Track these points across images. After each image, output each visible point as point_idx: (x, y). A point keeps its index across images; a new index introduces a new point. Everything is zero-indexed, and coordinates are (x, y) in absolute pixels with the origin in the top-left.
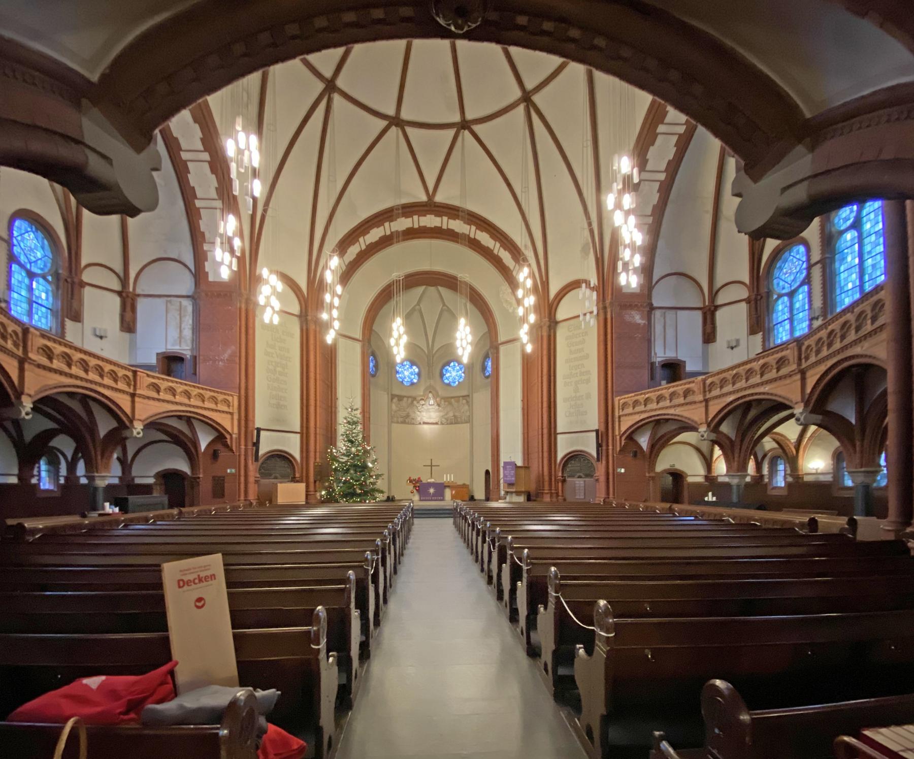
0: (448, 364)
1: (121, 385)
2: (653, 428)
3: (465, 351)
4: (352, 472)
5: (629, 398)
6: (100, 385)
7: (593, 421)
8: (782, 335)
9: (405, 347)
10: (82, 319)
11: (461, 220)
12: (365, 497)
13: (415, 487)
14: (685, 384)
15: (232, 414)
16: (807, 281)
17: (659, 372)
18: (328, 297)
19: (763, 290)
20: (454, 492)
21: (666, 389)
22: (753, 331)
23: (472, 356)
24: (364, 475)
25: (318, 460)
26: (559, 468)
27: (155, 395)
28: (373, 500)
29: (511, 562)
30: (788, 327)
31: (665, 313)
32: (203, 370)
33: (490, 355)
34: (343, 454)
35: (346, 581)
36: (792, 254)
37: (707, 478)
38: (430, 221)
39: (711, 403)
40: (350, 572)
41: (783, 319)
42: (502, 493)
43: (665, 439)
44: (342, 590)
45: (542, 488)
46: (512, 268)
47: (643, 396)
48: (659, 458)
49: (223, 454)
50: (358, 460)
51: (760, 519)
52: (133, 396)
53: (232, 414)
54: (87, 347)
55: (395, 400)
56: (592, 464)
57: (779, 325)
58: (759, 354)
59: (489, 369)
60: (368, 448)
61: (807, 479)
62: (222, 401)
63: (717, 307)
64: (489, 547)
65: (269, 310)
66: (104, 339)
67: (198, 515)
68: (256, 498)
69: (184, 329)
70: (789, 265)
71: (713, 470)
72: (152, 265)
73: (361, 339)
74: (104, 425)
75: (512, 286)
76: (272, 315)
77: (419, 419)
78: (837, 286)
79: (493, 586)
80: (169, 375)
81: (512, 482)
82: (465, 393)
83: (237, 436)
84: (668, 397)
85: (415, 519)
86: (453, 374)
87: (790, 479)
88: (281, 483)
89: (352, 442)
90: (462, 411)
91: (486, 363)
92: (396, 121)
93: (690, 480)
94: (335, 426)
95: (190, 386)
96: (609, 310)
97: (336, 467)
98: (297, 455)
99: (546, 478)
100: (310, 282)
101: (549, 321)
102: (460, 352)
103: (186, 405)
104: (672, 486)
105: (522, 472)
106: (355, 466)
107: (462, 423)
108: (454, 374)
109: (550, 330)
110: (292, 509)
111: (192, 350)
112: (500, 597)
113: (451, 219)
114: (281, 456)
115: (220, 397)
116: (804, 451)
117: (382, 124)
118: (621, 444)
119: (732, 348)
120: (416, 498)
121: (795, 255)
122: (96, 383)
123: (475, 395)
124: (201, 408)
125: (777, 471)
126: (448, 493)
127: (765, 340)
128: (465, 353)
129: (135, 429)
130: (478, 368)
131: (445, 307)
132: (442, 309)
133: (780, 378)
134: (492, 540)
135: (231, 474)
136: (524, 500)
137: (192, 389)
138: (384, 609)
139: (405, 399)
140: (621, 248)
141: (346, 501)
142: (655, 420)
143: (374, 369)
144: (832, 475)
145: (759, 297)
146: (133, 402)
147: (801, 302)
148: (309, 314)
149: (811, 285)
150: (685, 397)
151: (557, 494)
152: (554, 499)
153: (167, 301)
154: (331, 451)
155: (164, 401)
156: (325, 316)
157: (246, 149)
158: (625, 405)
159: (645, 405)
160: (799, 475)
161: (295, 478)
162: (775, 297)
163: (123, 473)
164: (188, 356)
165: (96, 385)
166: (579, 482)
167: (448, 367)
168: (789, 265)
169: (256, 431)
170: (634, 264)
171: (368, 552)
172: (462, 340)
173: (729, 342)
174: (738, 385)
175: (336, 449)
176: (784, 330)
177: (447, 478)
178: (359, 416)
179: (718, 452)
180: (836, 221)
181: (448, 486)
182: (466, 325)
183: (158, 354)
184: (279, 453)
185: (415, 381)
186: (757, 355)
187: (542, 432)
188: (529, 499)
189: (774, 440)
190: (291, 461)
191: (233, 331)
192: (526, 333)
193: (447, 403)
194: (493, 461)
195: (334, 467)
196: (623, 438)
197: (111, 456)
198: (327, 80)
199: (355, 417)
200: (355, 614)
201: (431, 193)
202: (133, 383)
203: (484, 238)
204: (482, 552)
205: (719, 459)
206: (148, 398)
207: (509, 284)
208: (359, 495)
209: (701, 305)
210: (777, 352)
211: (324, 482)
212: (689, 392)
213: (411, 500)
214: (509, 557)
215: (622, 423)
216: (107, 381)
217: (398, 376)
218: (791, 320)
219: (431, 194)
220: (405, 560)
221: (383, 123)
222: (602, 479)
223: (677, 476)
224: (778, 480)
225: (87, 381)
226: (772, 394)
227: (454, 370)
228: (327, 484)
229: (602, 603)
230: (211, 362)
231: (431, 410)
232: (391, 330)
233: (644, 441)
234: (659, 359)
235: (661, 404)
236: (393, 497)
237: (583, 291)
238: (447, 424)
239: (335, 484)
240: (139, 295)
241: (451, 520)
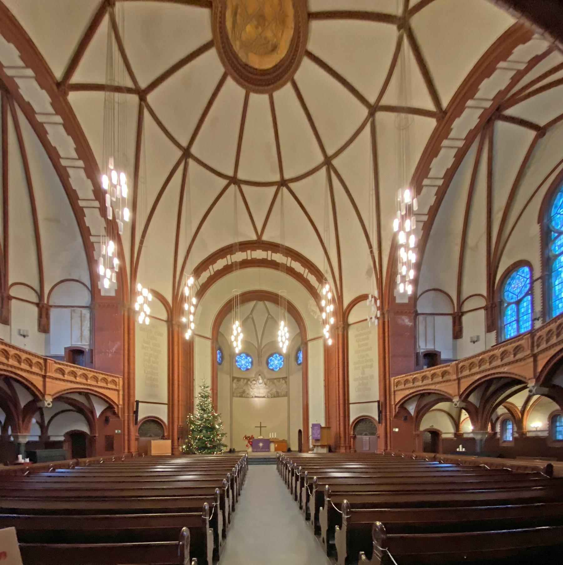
0: (272, 355)
1: (35, 369)
2: (419, 399)
5: (401, 378)
6: (19, 369)
7: (375, 394)
8: (511, 332)
10: (10, 324)
11: (281, 253)
12: (213, 450)
13: (249, 442)
14: (443, 367)
15: (118, 391)
16: (531, 292)
17: (422, 360)
18: (186, 306)
19: (497, 300)
20: (276, 446)
21: (428, 371)
22: (489, 329)
23: (290, 348)
24: (213, 434)
25: (180, 424)
26: (351, 428)
27: (61, 376)
28: (220, 452)
29: (328, 507)
30: (515, 326)
31: (426, 318)
33: (302, 349)
34: (198, 419)
35: (201, 509)
36: (519, 273)
37: (456, 435)
38: (259, 254)
39: (462, 381)
40: (205, 504)
41: (512, 321)
42: (311, 446)
43: (427, 407)
44: (177, 546)
45: (339, 443)
46: (316, 287)
47: (411, 376)
48: (422, 421)
49: (112, 419)
50: (209, 423)
51: (511, 466)
52: (44, 377)
53: (118, 391)
54: (13, 343)
55: (235, 381)
56: (375, 425)
57: (508, 325)
58: (494, 346)
60: (216, 415)
61: (529, 435)
62: (110, 381)
63: (463, 314)
66: (26, 338)
67: (90, 464)
68: (137, 451)
69: (84, 330)
70: (516, 282)
72: (60, 285)
73: (211, 338)
74: (24, 400)
75: (317, 300)
76: (145, 318)
77: (252, 394)
78: (553, 295)
79: (297, 501)
80: (74, 363)
82: (284, 376)
83: (122, 406)
84: (430, 376)
86: (276, 362)
87: (516, 435)
88: (154, 440)
90: (282, 388)
91: (298, 355)
92: (234, 180)
93: (444, 436)
95: (87, 370)
96: (386, 316)
97: (193, 429)
98: (165, 420)
99: (342, 435)
101: (343, 324)
102: (281, 345)
103: (84, 384)
104: (431, 441)
105: (325, 431)
106: (206, 428)
109: (344, 330)
110: (161, 459)
111: (90, 345)
112: (308, 518)
113: (274, 252)
114: (154, 421)
115: (110, 379)
116: (527, 415)
117: (225, 182)
118: (395, 411)
119: (474, 342)
120: (250, 450)
121: (521, 274)
122: (15, 367)
123: (291, 377)
124: (96, 386)
125: (506, 429)
126: (272, 446)
127: (498, 336)
130: (293, 358)
131: (270, 316)
133: (517, 361)
135: (118, 434)
136: (327, 451)
137: (89, 372)
138: (223, 544)
139: (242, 380)
140: (399, 265)
141: (200, 453)
143: (220, 359)
144: (548, 432)
145: (494, 305)
146: (44, 382)
147: (525, 308)
149: (534, 295)
150: (443, 377)
152: (348, 451)
153: (71, 310)
154: (190, 416)
155: (67, 381)
156: (184, 320)
158: (397, 384)
159: (413, 383)
160: (523, 432)
161: (164, 436)
162: (506, 305)
163: (42, 432)
164: (87, 350)
165: (15, 369)
166: (366, 438)
167: (272, 358)
168: (516, 282)
171: (217, 489)
172: (282, 336)
173: (471, 338)
174: (483, 367)
175: (193, 415)
176: (512, 329)
177: (272, 436)
178: (210, 392)
179: (464, 415)
180: (553, 248)
181: (273, 442)
182: (285, 326)
183: (65, 348)
184: (153, 419)
185: (249, 367)
186: (492, 347)
187: (339, 402)
188: (330, 451)
189: (505, 407)
191: (119, 331)
192: (327, 331)
194: (304, 424)
195: (191, 428)
196: (397, 406)
197: (30, 421)
198: (184, 149)
199: (207, 392)
200: (210, 532)
201: (259, 234)
202: (44, 368)
203: (297, 266)
204: (292, 481)
205: (466, 420)
206: (56, 379)
208: (209, 448)
209: (451, 312)
210: (515, 342)
211: (185, 439)
212: (446, 372)
213: (246, 451)
214: (326, 503)
215: (396, 396)
216: (24, 366)
217: (237, 364)
218: (518, 321)
223: (435, 434)
224: (507, 436)
225: (8, 365)
226: (510, 373)
227: (276, 359)
228: (187, 440)
229: (378, 523)
230: (103, 354)
232: (232, 330)
233: (412, 409)
234: (422, 351)
235: (425, 382)
236: (234, 449)
237: (369, 302)
238: (272, 397)
239: (192, 441)
240: (51, 306)
241: (275, 466)
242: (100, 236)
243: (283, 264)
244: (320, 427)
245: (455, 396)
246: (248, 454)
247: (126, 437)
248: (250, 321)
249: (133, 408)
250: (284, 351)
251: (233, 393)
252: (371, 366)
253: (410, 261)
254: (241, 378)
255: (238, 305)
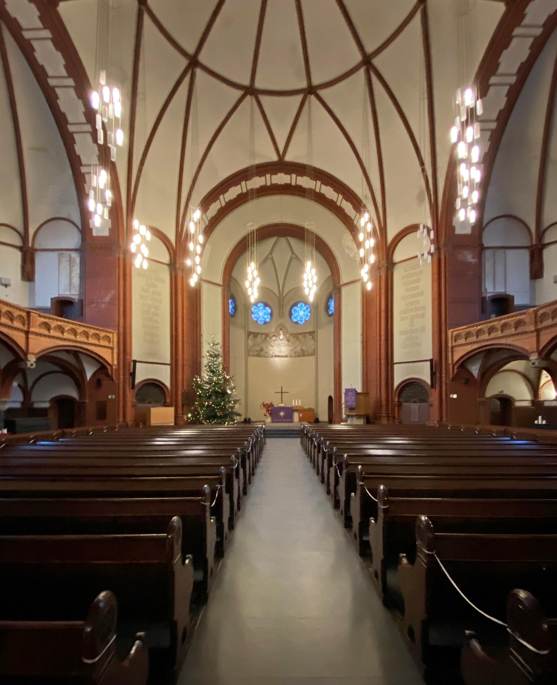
0: (296, 305)
1: (17, 324)
3: (311, 291)
4: (214, 397)
5: (462, 330)
9: (258, 288)
13: (268, 410)
15: (112, 348)
17: (489, 307)
18: (191, 246)
20: (301, 415)
21: (497, 322)
23: (318, 296)
24: (224, 401)
25: (185, 388)
26: (395, 394)
27: (46, 332)
29: (361, 494)
32: (88, 311)
37: (533, 402)
38: (281, 179)
39: (542, 333)
42: (344, 416)
46: (353, 217)
47: (475, 328)
49: (105, 382)
52: (27, 333)
55: (251, 336)
59: (332, 308)
64: (336, 472)
65: (139, 257)
66: (8, 288)
71: (539, 396)
73: (222, 284)
76: (142, 261)
77: (271, 352)
80: (61, 316)
81: (353, 407)
82: (311, 330)
85: (267, 439)
89: (212, 372)
93: (518, 404)
94: (201, 359)
97: (200, 394)
98: (168, 383)
99: (384, 403)
100: (178, 235)
102: (306, 291)
107: (308, 355)
108: (302, 313)
109: (387, 271)
110: (162, 430)
111: (80, 294)
117: (239, 93)
120: (269, 420)
124: (85, 343)
126: (296, 416)
128: (311, 293)
129: (29, 361)
131: (294, 256)
132: (291, 257)
134: (338, 465)
135: (111, 399)
136: (364, 423)
139: (259, 336)
140: (459, 186)
141: (209, 423)
142: (485, 350)
143: (233, 310)
146: (27, 339)
148: (177, 262)
151: (394, 417)
153: (59, 255)
154: (196, 379)
155: (53, 337)
156: (188, 262)
157: (110, 102)
163: (25, 398)
164: (76, 300)
166: (415, 407)
167: (296, 308)
169: (132, 363)
170: (472, 201)
172: (308, 281)
177: (296, 403)
179: (545, 377)
181: (296, 410)
182: (311, 268)
183: (52, 299)
185: (268, 320)
188: (368, 421)
190: (162, 388)
192: (367, 273)
193: (295, 339)
195: (198, 393)
196: (456, 367)
199: (217, 351)
202: (27, 322)
203: (329, 192)
207: (350, 231)
208: (220, 417)
217: (253, 316)
219: (281, 155)
220: (256, 480)
221: (239, 93)
222: (436, 403)
231: (281, 345)
233: (475, 369)
234: (489, 295)
235: (493, 335)
236: (250, 419)
237: (421, 234)
241: (298, 440)
242: (90, 165)
243: (310, 190)
244: (355, 393)
245: (532, 352)
246: (266, 425)
247: (121, 404)
248: (269, 262)
249: (129, 370)
250: (311, 299)
251: (249, 352)
252: (423, 316)
253: (474, 179)
254: (258, 334)
255: (254, 243)
